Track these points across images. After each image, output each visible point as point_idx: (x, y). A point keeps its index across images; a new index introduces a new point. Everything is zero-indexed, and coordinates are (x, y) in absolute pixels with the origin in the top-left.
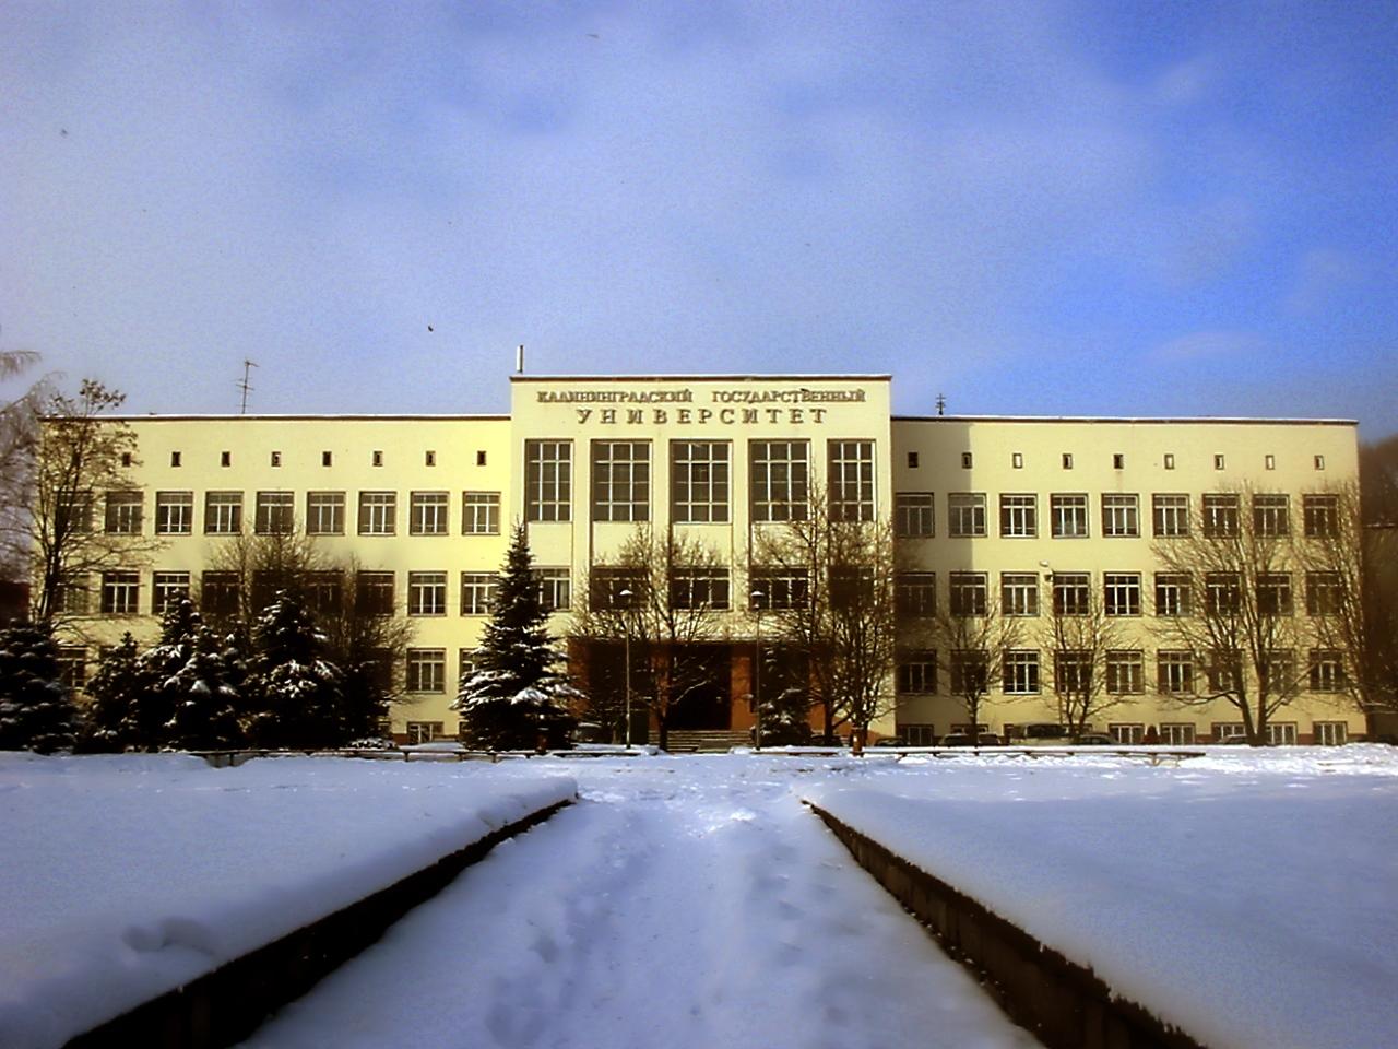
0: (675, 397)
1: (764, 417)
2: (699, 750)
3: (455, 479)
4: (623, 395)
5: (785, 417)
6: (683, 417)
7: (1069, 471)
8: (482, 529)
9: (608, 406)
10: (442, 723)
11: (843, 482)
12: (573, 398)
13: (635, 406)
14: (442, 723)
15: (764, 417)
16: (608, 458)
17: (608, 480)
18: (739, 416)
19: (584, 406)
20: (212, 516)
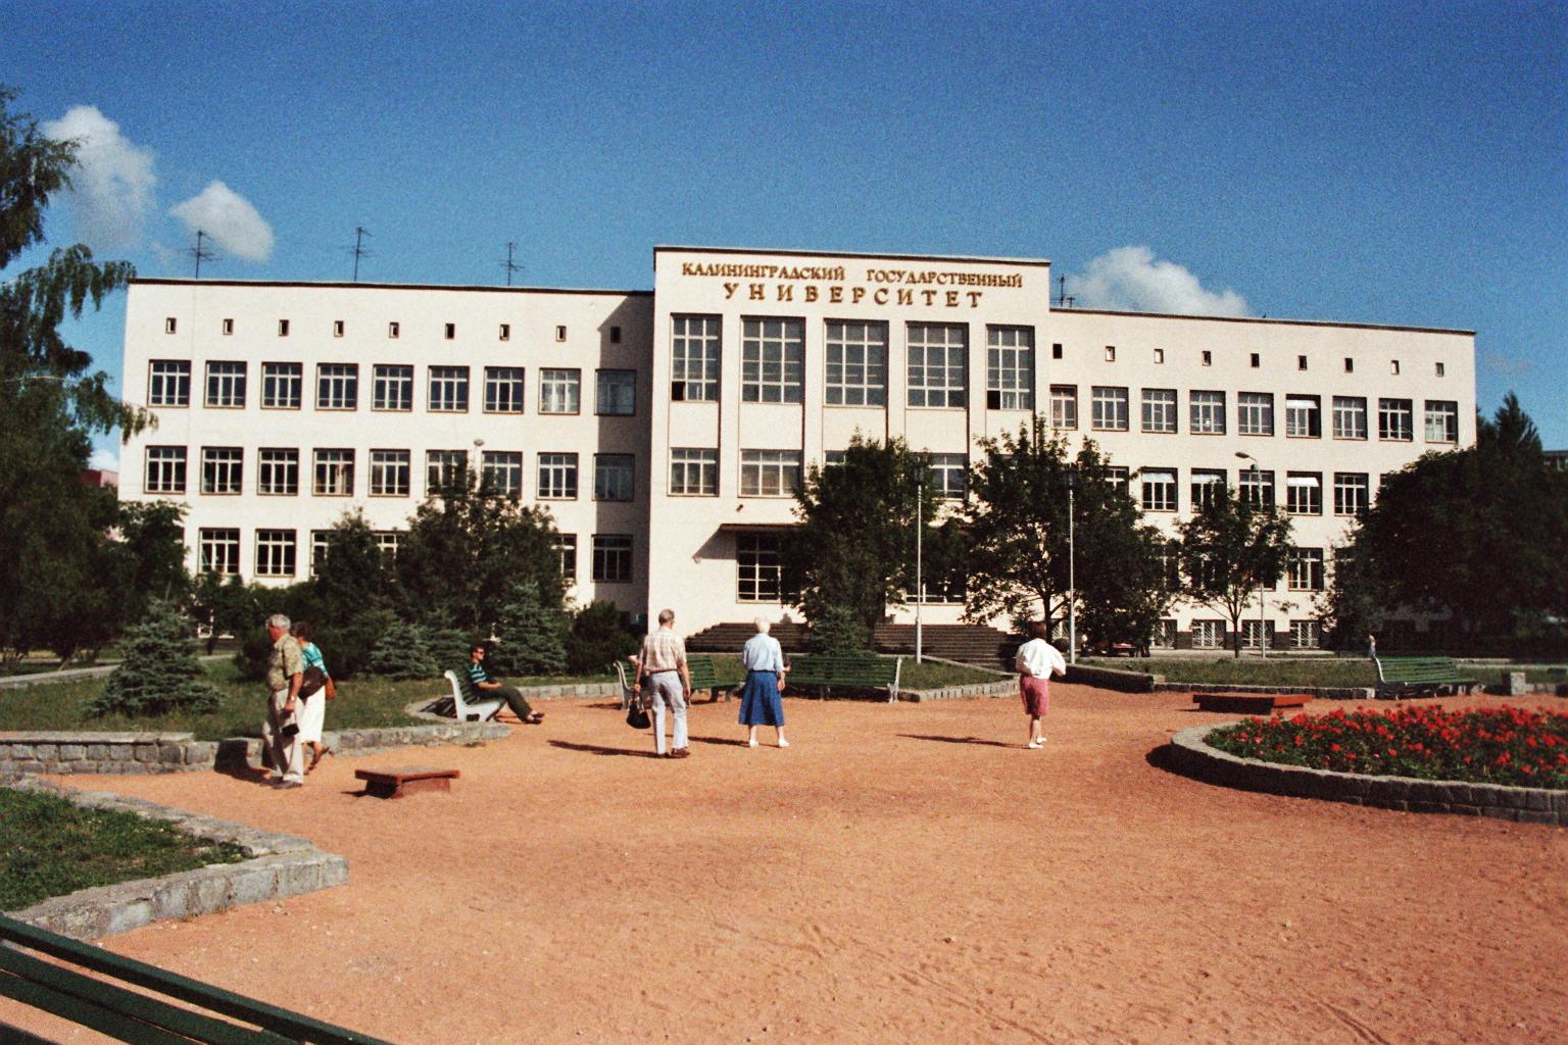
0: (828, 274)
1: (919, 299)
2: (98, 661)
3: (531, 353)
4: (773, 269)
5: (940, 299)
6: (836, 294)
7: (171, 317)
9: (757, 281)
10: (575, 535)
11: (704, 359)
12: (713, 272)
13: (786, 283)
14: (575, 535)
15: (940, 299)
18: (893, 296)
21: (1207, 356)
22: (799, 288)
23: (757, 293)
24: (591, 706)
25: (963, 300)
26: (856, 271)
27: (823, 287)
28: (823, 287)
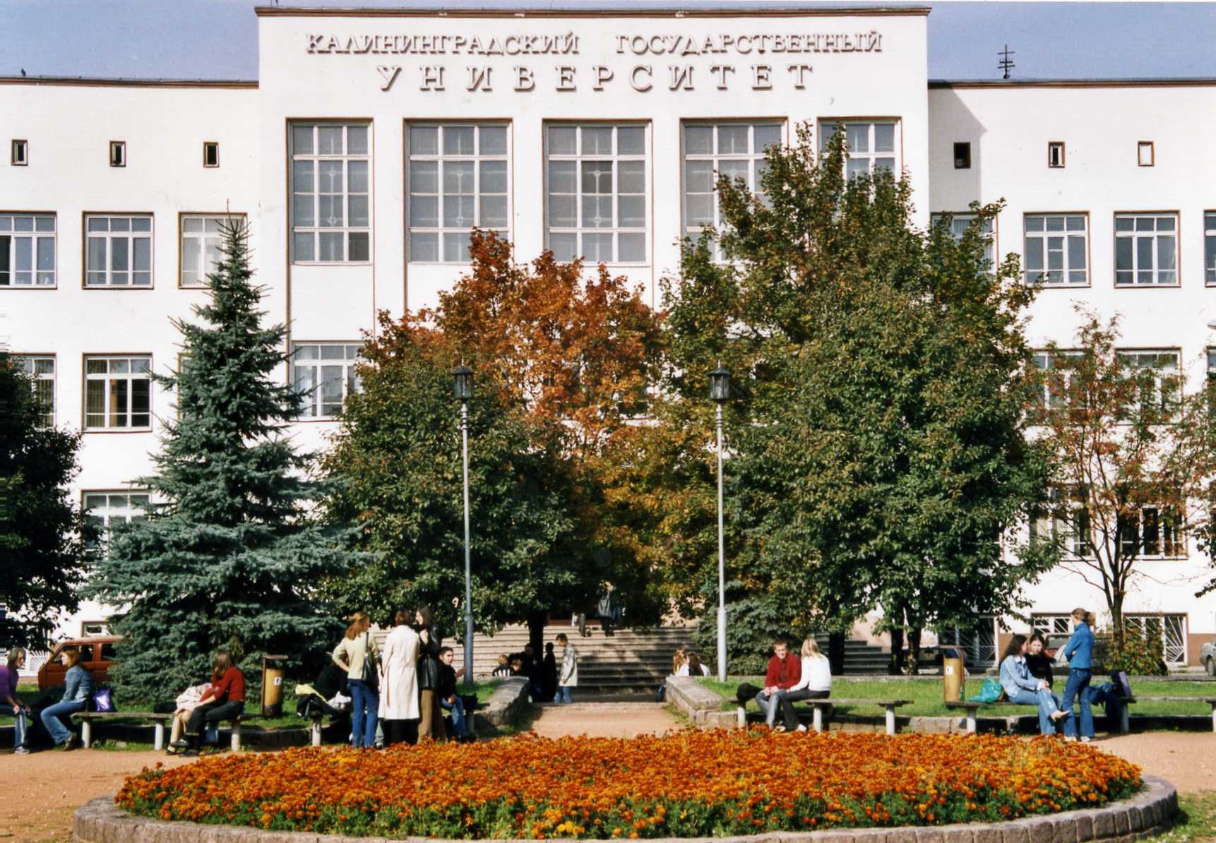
5: (744, 78)
8: (1144, 277)
13: (481, 63)
15: (704, 80)
16: (311, 152)
17: (575, 191)
19: (391, 61)
20: (95, 257)
21: (117, 158)
22: (504, 73)
23: (432, 83)
24: (904, 702)
25: (781, 79)
26: (597, 37)
27: (545, 70)
28: (545, 70)
